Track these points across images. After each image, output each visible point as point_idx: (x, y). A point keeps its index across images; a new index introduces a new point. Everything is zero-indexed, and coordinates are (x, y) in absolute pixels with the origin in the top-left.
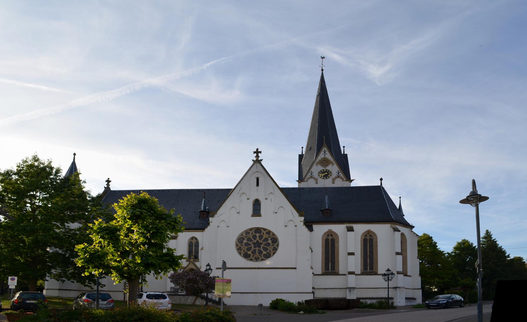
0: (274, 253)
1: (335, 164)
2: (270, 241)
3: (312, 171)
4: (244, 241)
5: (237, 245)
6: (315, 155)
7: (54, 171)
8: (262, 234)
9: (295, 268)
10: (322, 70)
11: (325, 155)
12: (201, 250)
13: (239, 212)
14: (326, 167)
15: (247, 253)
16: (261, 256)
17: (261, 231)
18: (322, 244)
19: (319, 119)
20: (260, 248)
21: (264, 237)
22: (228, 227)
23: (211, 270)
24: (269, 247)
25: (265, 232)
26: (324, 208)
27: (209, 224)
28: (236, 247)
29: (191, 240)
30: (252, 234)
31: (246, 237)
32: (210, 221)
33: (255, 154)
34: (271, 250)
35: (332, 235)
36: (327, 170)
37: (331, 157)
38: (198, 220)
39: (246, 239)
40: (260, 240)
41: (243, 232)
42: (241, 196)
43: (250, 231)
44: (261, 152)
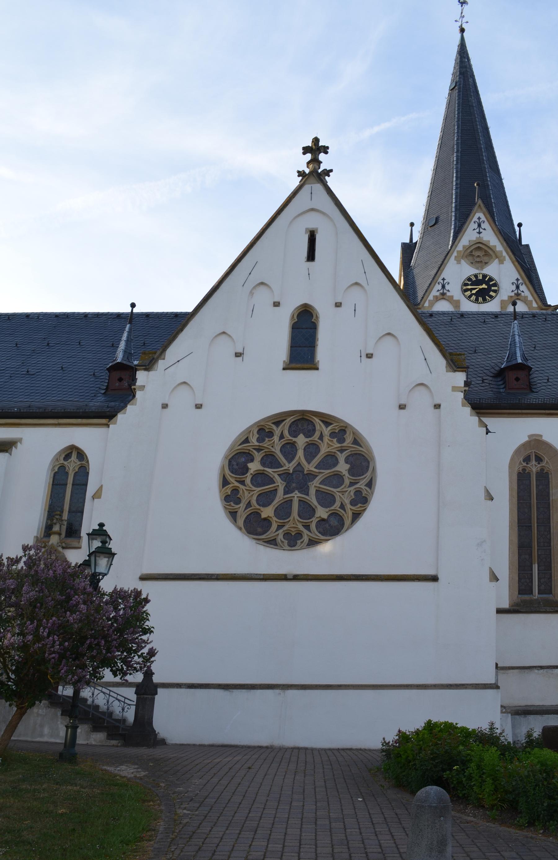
0: (356, 516)
1: (507, 258)
2: (343, 467)
3: (444, 279)
4: (250, 465)
5: (225, 482)
6: (452, 235)
7: (145, 651)
8: (316, 437)
9: (434, 579)
10: (462, 30)
11: (479, 233)
12: (93, 498)
13: (240, 351)
14: (482, 269)
15: (257, 514)
16: (307, 527)
17: (314, 426)
18: (511, 489)
19: (457, 144)
20: (308, 495)
21: (324, 450)
22: (199, 407)
23: (111, 555)
24: (338, 490)
25: (327, 431)
26: (510, 364)
27: (133, 395)
28: (220, 491)
29: (62, 461)
30: (282, 437)
31: (259, 450)
32: (139, 383)
33: (309, 156)
34: (347, 501)
35: (539, 459)
36: (484, 276)
37: (497, 241)
38: (101, 398)
39: (258, 456)
40: (309, 463)
41: (249, 431)
42: (251, 293)
43: (274, 427)
44: (328, 148)
